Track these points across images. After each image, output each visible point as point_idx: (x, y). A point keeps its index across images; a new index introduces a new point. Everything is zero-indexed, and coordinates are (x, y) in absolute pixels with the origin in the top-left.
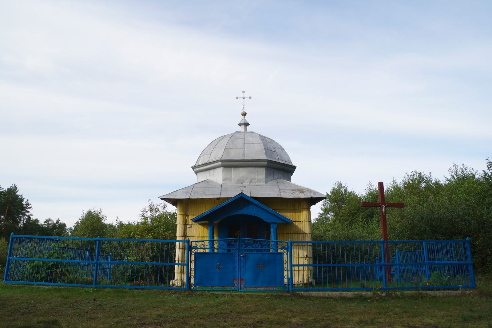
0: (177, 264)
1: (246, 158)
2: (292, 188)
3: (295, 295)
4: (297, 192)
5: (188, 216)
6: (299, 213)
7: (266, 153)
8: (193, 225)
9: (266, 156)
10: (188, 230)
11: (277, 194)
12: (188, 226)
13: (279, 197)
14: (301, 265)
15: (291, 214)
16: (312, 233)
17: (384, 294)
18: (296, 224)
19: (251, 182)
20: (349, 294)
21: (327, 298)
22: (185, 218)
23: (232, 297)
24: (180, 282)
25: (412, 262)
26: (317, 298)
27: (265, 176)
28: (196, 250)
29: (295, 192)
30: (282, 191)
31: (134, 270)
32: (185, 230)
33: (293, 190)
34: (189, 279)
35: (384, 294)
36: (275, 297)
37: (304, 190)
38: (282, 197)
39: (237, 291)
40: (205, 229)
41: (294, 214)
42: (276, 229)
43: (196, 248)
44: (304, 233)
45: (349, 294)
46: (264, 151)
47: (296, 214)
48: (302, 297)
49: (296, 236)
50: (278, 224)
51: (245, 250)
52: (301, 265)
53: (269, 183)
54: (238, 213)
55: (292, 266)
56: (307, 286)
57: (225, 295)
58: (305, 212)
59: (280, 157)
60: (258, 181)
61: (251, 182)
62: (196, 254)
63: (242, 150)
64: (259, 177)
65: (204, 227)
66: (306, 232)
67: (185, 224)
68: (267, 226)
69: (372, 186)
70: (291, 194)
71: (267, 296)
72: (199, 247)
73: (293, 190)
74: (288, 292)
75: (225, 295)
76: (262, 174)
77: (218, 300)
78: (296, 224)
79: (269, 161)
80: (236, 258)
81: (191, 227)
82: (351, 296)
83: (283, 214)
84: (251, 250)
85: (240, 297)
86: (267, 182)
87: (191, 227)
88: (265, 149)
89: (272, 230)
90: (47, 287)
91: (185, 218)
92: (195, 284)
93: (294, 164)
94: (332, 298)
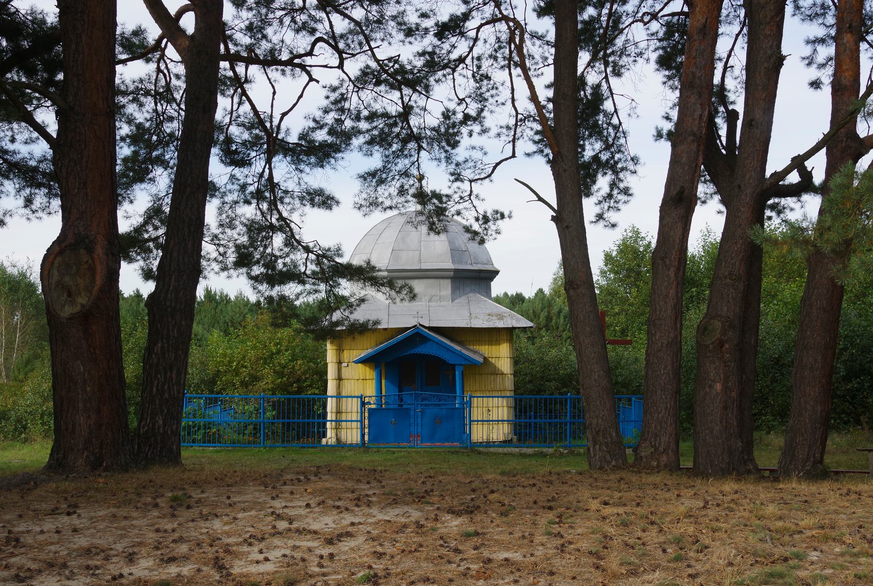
0: (329, 421)
1: (424, 266)
2: (488, 312)
3: (473, 451)
4: (494, 318)
5: (343, 350)
6: (497, 347)
7: (453, 256)
8: (350, 364)
9: (453, 262)
10: (343, 370)
11: (465, 321)
12: (344, 365)
13: (469, 326)
14: (480, 421)
15: (487, 347)
16: (515, 374)
17: (566, 452)
18: (493, 361)
19: (430, 301)
20: (530, 451)
21: (506, 454)
22: (339, 354)
23: (409, 453)
24: (334, 440)
25: (579, 416)
26: (495, 454)
27: (450, 292)
28: (370, 406)
29: (491, 318)
30: (473, 316)
31: (287, 426)
32: (339, 370)
33: (489, 315)
34: (363, 435)
35: (566, 452)
36: (452, 453)
37: (504, 314)
38: (473, 326)
39: (414, 447)
40: (368, 369)
41: (490, 347)
42: (462, 372)
43: (369, 403)
44: (502, 374)
45: (530, 451)
46: (449, 255)
47: (494, 347)
48: (480, 453)
49: (492, 377)
50: (465, 366)
51: (422, 405)
52: (480, 421)
53: (456, 301)
54: (413, 351)
55: (471, 421)
56: (506, 443)
57: (401, 452)
58: (505, 344)
59: (475, 258)
60: (441, 299)
61: (430, 301)
62: (369, 409)
63: (417, 252)
64: (443, 293)
65: (365, 366)
66: (505, 372)
67: (340, 363)
68: (453, 367)
69: (712, 234)
70: (485, 322)
71: (444, 452)
72: (372, 402)
73: (489, 315)
74: (466, 448)
75: (401, 452)
76: (446, 288)
77: (395, 455)
78: (493, 362)
79: (456, 271)
80: (412, 413)
81: (348, 365)
82: (531, 453)
83: (475, 347)
84: (426, 405)
85: (416, 452)
86: (453, 301)
87: (348, 365)
88: (451, 250)
89: (457, 373)
90: (211, 449)
91: (339, 354)
92: (369, 441)
93: (497, 266)
94: (510, 454)
